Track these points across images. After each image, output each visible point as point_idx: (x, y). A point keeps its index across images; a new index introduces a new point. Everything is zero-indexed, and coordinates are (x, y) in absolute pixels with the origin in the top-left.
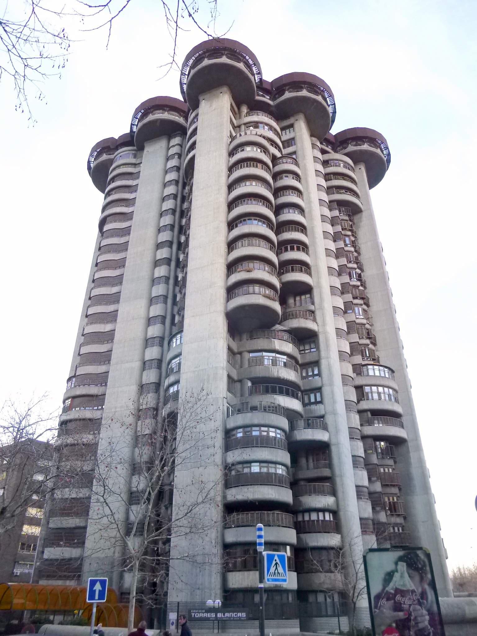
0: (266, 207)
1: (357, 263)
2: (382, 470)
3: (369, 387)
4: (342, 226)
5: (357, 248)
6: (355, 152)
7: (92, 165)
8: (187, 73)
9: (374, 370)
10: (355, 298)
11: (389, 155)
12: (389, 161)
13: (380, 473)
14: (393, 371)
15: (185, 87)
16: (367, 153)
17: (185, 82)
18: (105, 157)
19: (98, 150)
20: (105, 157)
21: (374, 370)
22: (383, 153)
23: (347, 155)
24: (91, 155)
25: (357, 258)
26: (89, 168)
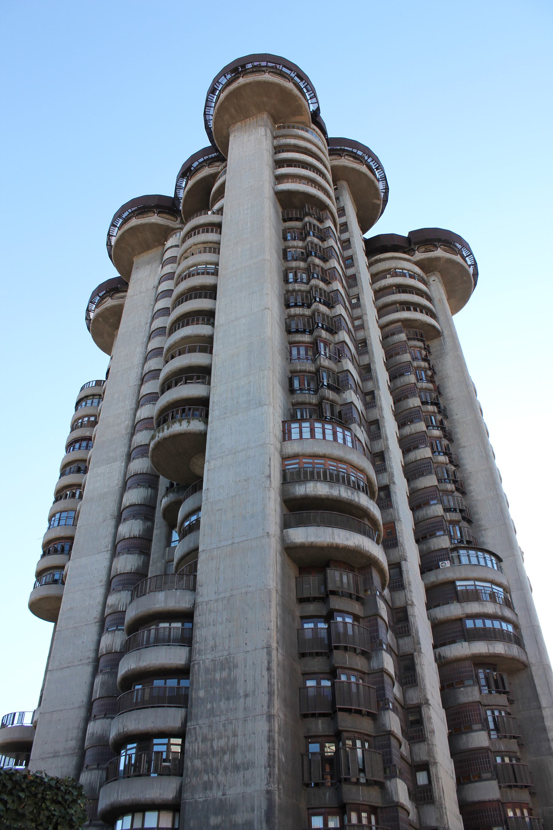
1: (455, 482)
2: (499, 760)
4: (421, 399)
5: (453, 456)
9: (468, 556)
10: (424, 403)
11: (475, 265)
12: (476, 274)
13: (496, 766)
14: (499, 559)
16: (444, 262)
18: (109, 302)
20: (109, 302)
21: (468, 556)
22: (466, 262)
23: (417, 263)
24: (91, 302)
26: (88, 319)
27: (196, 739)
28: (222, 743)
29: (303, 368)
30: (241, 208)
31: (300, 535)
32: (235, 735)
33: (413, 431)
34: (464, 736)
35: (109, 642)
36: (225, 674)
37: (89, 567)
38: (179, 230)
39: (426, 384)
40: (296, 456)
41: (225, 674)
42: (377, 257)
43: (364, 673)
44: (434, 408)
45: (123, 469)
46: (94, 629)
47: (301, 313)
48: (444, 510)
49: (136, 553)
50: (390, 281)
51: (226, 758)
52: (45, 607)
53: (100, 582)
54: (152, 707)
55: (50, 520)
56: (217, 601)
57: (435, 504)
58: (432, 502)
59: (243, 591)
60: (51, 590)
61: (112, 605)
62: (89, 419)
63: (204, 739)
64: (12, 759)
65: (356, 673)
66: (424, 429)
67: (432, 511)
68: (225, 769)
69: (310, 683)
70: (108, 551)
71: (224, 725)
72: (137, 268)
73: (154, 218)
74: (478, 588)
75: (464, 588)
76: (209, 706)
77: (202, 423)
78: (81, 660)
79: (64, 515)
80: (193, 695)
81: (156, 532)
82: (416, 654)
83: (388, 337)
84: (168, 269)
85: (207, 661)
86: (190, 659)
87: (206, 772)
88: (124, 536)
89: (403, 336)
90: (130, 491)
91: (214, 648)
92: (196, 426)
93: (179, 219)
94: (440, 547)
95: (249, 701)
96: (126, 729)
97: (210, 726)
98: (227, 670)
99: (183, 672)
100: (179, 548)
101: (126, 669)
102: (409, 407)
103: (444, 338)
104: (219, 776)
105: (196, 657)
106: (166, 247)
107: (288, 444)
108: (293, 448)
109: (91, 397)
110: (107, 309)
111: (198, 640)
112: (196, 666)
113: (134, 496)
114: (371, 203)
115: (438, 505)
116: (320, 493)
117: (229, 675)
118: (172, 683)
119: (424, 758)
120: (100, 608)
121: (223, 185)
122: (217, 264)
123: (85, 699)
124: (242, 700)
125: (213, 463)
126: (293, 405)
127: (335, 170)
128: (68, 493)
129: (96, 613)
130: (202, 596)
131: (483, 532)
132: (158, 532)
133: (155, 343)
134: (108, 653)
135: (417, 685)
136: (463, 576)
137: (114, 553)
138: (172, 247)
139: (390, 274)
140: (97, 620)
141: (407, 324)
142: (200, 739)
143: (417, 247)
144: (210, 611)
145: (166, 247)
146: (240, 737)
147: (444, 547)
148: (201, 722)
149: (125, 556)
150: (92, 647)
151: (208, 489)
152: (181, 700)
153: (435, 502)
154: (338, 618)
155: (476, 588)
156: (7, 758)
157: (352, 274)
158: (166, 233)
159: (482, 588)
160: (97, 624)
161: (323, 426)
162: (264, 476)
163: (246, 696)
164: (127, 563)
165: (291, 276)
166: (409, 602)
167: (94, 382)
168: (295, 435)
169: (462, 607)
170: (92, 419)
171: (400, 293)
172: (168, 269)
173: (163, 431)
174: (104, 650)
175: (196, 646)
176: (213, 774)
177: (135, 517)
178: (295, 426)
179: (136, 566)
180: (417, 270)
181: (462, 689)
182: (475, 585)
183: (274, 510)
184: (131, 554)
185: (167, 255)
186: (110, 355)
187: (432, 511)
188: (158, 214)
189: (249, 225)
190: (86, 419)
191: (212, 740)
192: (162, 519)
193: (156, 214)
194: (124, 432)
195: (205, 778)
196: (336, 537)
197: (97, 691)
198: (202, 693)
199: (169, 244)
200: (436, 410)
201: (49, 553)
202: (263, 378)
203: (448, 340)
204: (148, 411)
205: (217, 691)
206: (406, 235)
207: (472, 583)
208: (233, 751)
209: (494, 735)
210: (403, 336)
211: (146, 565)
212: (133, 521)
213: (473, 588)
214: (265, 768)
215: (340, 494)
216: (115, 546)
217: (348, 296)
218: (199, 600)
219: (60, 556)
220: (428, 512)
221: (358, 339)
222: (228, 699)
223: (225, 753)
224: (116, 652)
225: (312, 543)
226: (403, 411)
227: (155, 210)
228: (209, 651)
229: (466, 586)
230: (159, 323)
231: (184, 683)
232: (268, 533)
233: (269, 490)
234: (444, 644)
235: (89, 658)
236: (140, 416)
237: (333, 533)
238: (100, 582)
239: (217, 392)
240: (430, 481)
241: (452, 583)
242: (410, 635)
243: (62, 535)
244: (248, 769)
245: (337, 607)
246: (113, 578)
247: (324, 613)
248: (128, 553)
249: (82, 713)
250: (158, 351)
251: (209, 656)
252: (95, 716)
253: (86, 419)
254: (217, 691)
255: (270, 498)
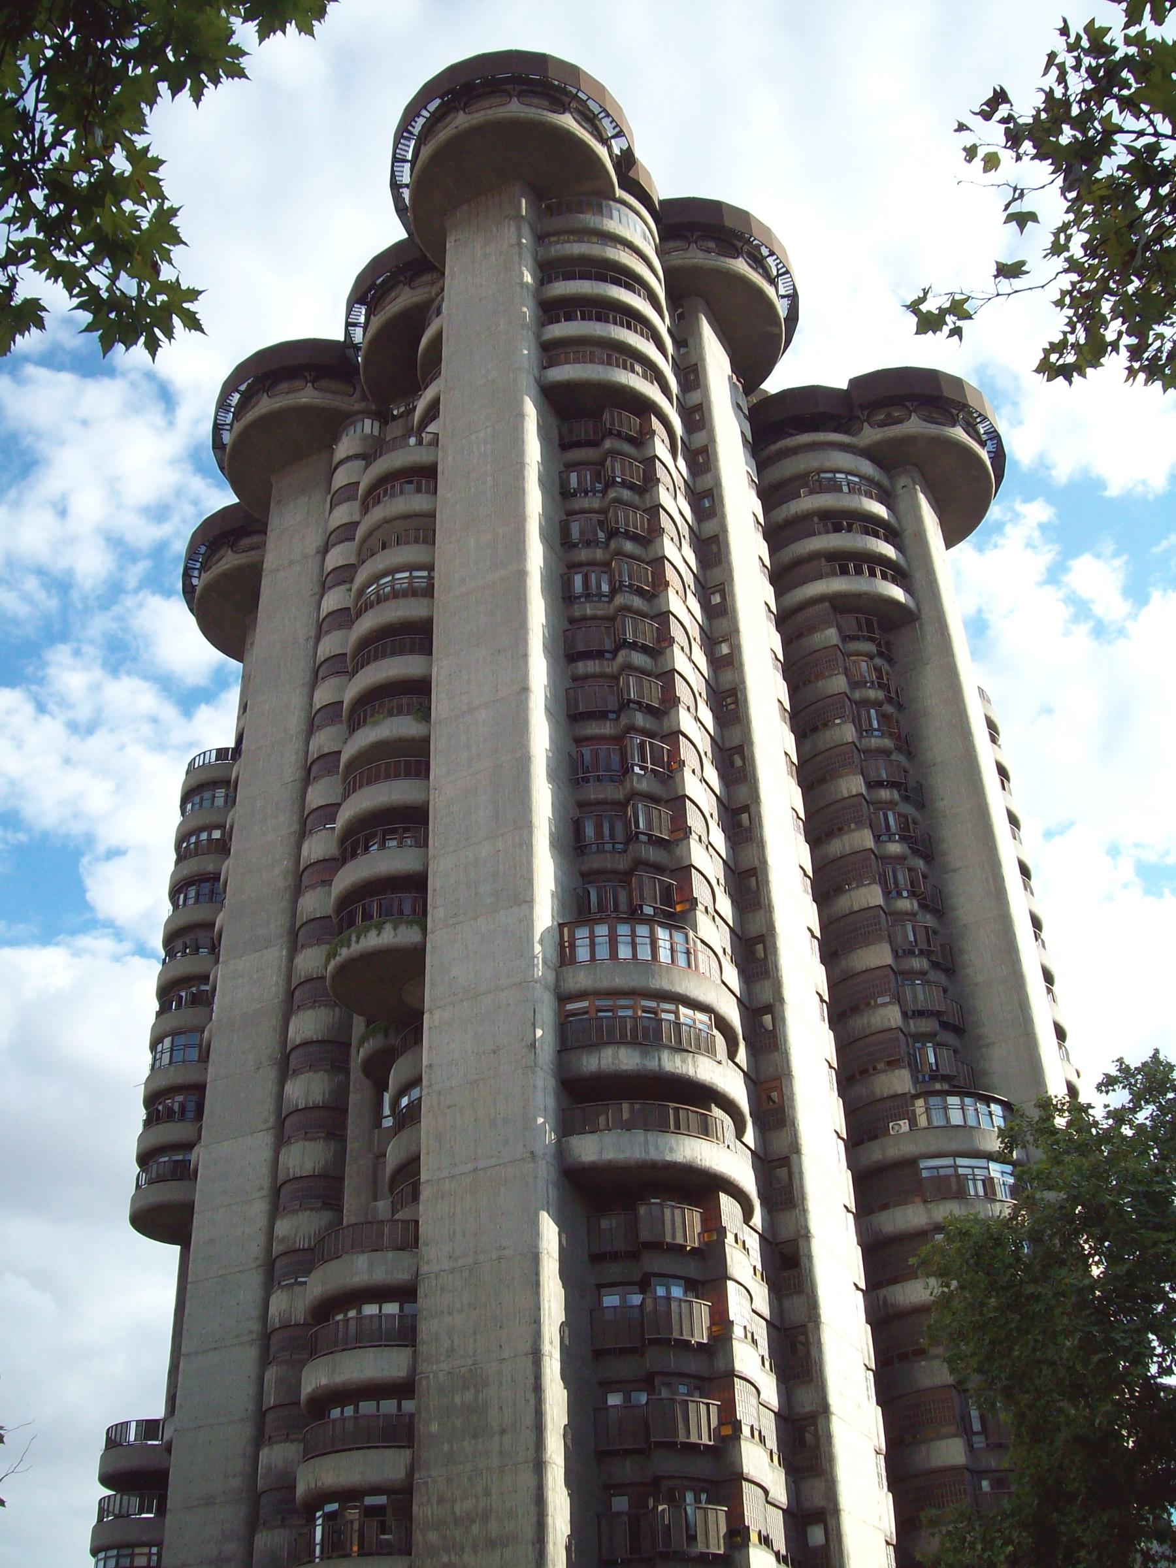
0: (642, 335)
3: (935, 1124)
6: (879, 444)
7: (227, 437)
8: (409, 157)
15: (406, 193)
17: (406, 179)
19: (243, 388)
20: (229, 560)
23: (867, 453)
25: (905, 823)
27: (429, 1498)
28: (468, 1505)
29: (602, 796)
30: (473, 437)
31: (591, 1149)
32: (487, 1493)
33: (848, 850)
34: (923, 1448)
35: (284, 1306)
36: (469, 1396)
37: (236, 1159)
38: (361, 416)
39: (877, 740)
40: (581, 995)
41: (469, 1396)
42: (781, 444)
43: (703, 1379)
44: (892, 794)
45: (284, 964)
46: (254, 1281)
47: (598, 670)
48: (905, 1014)
49: (319, 1138)
50: (808, 503)
51: (475, 1528)
52: (160, 1218)
53: (259, 1190)
54: (358, 1449)
55: (153, 1047)
56: (452, 1271)
57: (884, 1005)
58: (879, 1001)
59: (494, 1257)
60: (170, 1192)
61: (284, 1238)
62: (210, 835)
63: (441, 1500)
64: (133, 1499)
65: (686, 1380)
66: (870, 843)
67: (879, 1019)
68: (475, 1547)
69: (614, 1400)
70: (268, 1129)
71: (470, 1479)
72: (279, 502)
73: (307, 396)
74: (961, 1171)
75: (935, 1173)
76: (446, 1447)
77: (416, 928)
78: (237, 1336)
79: (181, 1040)
80: (421, 1429)
81: (353, 1098)
82: (810, 1325)
83: (800, 636)
84: (342, 514)
85: (441, 1374)
86: (413, 1369)
87: (447, 1550)
88: (297, 1105)
89: (831, 635)
90: (300, 1014)
91: (450, 1353)
92: (406, 936)
93: (358, 394)
94: (892, 1092)
95: (507, 1439)
96: (319, 1484)
97: (449, 1480)
98: (473, 1390)
99: (404, 1389)
100: (394, 1155)
101: (314, 1386)
102: (839, 797)
103: (921, 625)
104: (466, 1557)
105: (423, 1367)
106: (336, 460)
107: (568, 972)
108: (579, 980)
109: (210, 788)
110: (224, 574)
111: (425, 1337)
112: (424, 1383)
113: (307, 1025)
114: (759, 336)
115: (890, 1007)
116: (625, 1068)
117: (476, 1398)
118: (389, 1406)
119: (819, 1502)
120: (262, 1240)
121: (438, 339)
122: (430, 568)
123: (251, 1407)
124: (496, 1438)
125: (437, 1014)
126: (583, 875)
127: (672, 278)
128: (183, 994)
129: (255, 1249)
130: (428, 1262)
131: (984, 1050)
132: (358, 1098)
133: (324, 695)
134: (285, 1327)
135: (811, 1380)
136: (933, 1149)
137: (275, 1211)
138: (348, 459)
139: (806, 485)
140: (259, 1263)
141: (840, 604)
142: (434, 1500)
143: (866, 413)
144: (442, 1289)
145: (336, 460)
146: (494, 1497)
147: (900, 1092)
148: (434, 1473)
149: (301, 1143)
150: (255, 1313)
151: (430, 1066)
152: (401, 1434)
153: (887, 999)
154: (658, 1288)
155: (956, 1171)
156: (125, 1497)
157: (712, 534)
158: (332, 425)
159: (969, 1171)
160: (261, 1270)
161: (633, 931)
162: (524, 1044)
163: (503, 1432)
164: (304, 1157)
165: (578, 580)
166: (803, 1232)
167: (214, 753)
168: (583, 954)
169: (928, 1211)
170: (216, 834)
171: (827, 532)
172: (342, 514)
173: (349, 947)
174: (277, 1320)
175: (422, 1349)
176: (456, 1554)
177: (312, 1066)
178: (582, 933)
179: (322, 1162)
180: (867, 468)
181: (923, 1363)
182: (956, 1167)
183: (542, 1107)
184: (311, 1140)
185: (341, 479)
186: (240, 659)
187: (879, 1019)
188: (313, 382)
189: (489, 483)
190: (204, 836)
191: (454, 1502)
192: (360, 1074)
193: (309, 385)
194: (281, 884)
195: (445, 1559)
196: (652, 1149)
197: (269, 1394)
198: (434, 1427)
199: (343, 448)
200: (896, 796)
201: (158, 1119)
202: (521, 845)
203: (929, 629)
204: (316, 903)
205: (458, 1423)
206: (845, 387)
207: (948, 1161)
208: (485, 1517)
209: (979, 1442)
210: (831, 635)
211: (340, 1158)
212: (311, 1074)
213: (951, 1171)
214: (533, 1544)
215: (660, 1065)
216: (281, 1122)
217: (703, 587)
218: (424, 1269)
219: (180, 1125)
220: (873, 1021)
221: (722, 689)
222: (475, 1437)
223: (474, 1521)
224: (297, 1325)
225: (610, 1161)
226: (828, 805)
227: (307, 374)
228: (442, 1358)
229: (937, 1168)
230: (330, 645)
231: (408, 1406)
232: (532, 1152)
233: (534, 1073)
234: (894, 1281)
235: (251, 1332)
236: (309, 856)
237: (646, 1142)
238: (259, 1190)
239: (441, 869)
240: (878, 956)
241: (910, 1163)
242: (802, 1292)
243: (180, 1081)
244: (507, 1546)
245: (656, 1270)
246: (286, 1117)
247: (637, 1278)
248: (306, 1139)
249: (248, 1431)
250: (332, 710)
251: (444, 1366)
252: (270, 1438)
253: (204, 836)
254: (458, 1423)
255: (535, 1087)
